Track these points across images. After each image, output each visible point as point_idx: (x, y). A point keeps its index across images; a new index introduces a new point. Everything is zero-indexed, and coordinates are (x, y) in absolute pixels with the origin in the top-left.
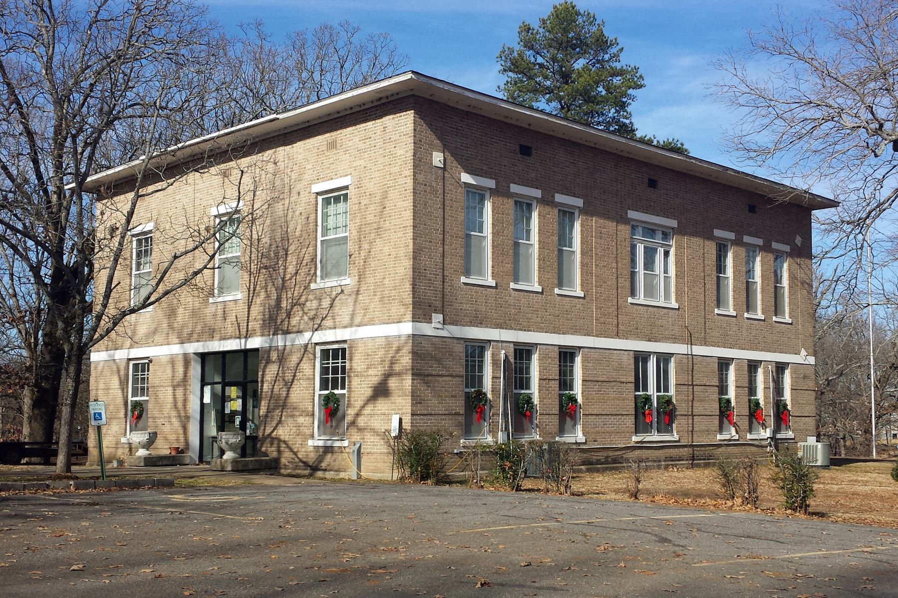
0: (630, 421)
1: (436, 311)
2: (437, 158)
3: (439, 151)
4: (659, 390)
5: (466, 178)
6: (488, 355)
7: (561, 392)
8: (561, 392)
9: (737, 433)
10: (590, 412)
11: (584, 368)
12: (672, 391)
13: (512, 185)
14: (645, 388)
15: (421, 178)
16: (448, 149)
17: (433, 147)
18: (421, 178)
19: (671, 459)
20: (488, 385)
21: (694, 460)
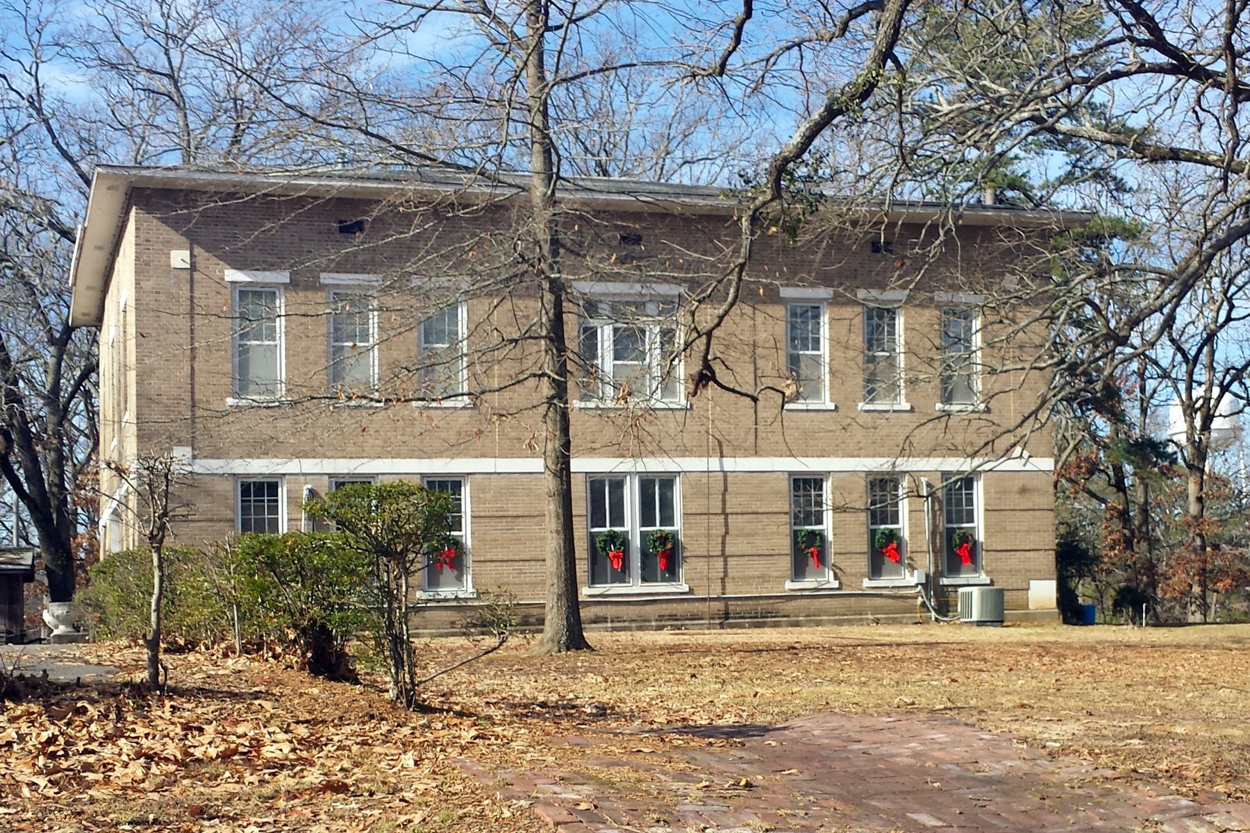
0: (786, 563)
1: (180, 443)
2: (179, 258)
3: (181, 248)
4: (647, 519)
5: (232, 275)
6: (283, 493)
7: (874, 527)
8: (874, 527)
9: (836, 577)
10: (489, 557)
11: (986, 492)
12: (678, 525)
13: (323, 275)
14: (618, 519)
15: (148, 285)
16: (200, 245)
17: (170, 245)
18: (148, 285)
19: (673, 617)
20: (904, 526)
21: (727, 618)
